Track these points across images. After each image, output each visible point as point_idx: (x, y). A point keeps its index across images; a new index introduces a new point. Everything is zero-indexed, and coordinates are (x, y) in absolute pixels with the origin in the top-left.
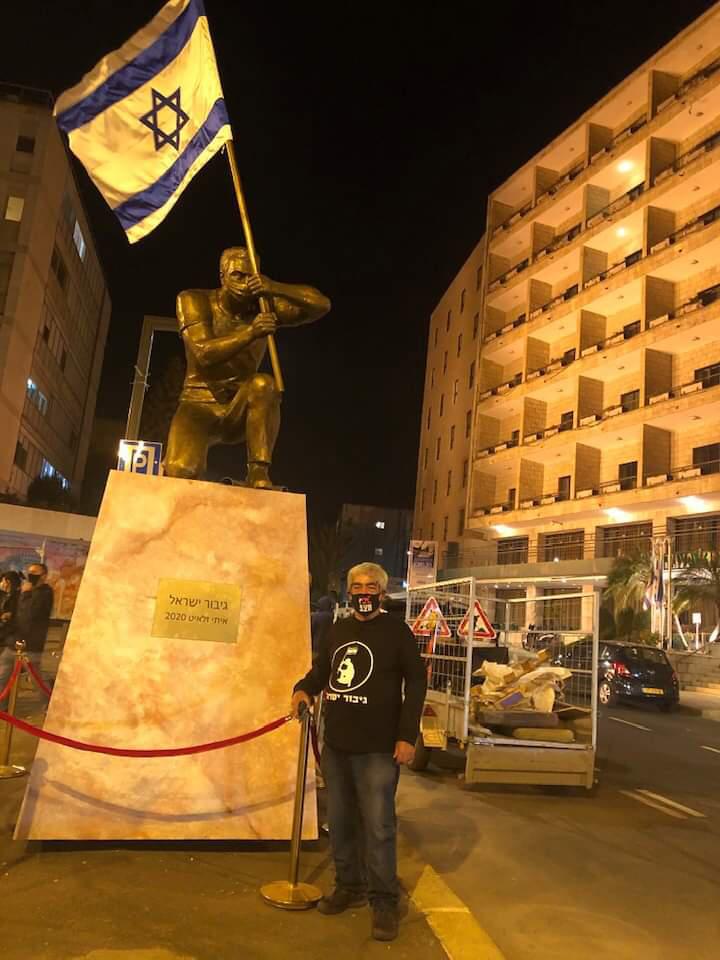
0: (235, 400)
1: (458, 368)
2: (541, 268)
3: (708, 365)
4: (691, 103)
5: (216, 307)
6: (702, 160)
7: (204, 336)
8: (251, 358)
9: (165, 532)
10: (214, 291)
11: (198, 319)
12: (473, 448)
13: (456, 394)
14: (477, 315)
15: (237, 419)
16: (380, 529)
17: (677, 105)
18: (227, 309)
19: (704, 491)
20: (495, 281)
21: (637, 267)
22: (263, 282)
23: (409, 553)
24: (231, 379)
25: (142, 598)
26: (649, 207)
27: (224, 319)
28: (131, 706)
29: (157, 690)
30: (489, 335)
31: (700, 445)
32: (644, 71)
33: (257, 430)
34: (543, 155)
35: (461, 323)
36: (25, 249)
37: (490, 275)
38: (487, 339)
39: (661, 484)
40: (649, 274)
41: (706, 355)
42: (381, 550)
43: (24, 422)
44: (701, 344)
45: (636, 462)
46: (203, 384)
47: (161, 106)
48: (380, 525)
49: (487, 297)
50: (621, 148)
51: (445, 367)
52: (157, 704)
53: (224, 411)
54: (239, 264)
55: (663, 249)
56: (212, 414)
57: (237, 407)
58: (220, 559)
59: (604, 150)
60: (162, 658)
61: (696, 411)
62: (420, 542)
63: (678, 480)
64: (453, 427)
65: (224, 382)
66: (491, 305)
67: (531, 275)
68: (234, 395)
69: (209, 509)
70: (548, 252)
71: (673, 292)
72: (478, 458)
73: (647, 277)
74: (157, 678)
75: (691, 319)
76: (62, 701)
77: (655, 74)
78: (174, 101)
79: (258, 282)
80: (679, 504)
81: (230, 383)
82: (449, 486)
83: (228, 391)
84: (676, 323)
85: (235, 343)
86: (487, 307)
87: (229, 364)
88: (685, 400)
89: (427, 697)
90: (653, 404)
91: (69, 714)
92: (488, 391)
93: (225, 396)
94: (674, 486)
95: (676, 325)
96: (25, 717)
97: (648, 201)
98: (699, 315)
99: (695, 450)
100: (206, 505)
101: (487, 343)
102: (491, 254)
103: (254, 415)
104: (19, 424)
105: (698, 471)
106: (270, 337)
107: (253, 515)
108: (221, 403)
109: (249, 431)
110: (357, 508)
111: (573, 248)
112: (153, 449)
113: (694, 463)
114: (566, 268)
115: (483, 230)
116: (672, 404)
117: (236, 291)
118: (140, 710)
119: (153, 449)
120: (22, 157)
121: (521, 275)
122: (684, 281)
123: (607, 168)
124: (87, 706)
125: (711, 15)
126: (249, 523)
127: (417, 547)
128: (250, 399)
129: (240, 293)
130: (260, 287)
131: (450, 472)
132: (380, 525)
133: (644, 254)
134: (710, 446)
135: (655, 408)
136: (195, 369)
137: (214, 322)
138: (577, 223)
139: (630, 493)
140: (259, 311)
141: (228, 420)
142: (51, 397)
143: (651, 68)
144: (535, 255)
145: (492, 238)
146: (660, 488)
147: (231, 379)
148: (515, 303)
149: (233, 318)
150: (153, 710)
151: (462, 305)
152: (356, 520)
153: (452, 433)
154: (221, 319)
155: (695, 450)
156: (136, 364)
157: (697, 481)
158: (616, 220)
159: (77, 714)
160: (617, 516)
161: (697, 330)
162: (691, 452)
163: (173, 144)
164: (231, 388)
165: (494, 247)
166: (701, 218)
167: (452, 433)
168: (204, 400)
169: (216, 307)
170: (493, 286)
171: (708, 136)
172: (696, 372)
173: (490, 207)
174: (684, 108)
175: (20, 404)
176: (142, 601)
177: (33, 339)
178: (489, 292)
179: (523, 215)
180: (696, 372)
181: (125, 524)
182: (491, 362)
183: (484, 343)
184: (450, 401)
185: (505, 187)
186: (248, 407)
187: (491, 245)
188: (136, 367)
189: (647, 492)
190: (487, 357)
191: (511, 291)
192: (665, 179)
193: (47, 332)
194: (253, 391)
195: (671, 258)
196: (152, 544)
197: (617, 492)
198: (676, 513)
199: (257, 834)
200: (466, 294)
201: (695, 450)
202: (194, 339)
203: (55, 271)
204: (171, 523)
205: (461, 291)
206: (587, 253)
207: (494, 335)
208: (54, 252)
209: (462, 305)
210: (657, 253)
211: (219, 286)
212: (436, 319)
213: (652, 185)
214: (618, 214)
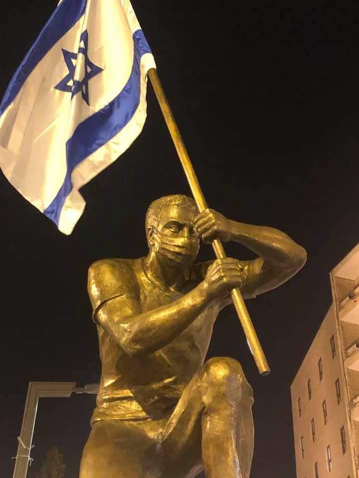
0: (179, 409)
1: (328, 435)
5: (143, 278)
7: (129, 312)
8: (193, 347)
10: (139, 261)
11: (121, 291)
13: (330, 461)
14: (338, 381)
15: (184, 440)
18: (157, 278)
20: (351, 346)
22: (216, 218)
24: (167, 381)
27: (156, 290)
33: (221, 450)
35: (323, 390)
37: (345, 342)
46: (128, 393)
49: (347, 361)
51: (314, 434)
53: (161, 430)
54: (165, 225)
56: (145, 438)
57: (183, 420)
65: (155, 386)
68: (176, 404)
79: (210, 219)
81: (166, 387)
83: (163, 399)
86: (348, 370)
87: (160, 353)
93: (160, 407)
96: (96, 305)
103: (213, 426)
106: (235, 291)
108: (154, 419)
109: (209, 452)
115: (330, 301)
117: (171, 249)
128: (206, 399)
129: (177, 250)
130: (213, 225)
136: (114, 370)
137: (142, 297)
140: (215, 258)
141: (168, 443)
145: (340, 308)
147: (167, 381)
149: (167, 290)
151: (321, 373)
154: (151, 291)
156: (19, 435)
164: (169, 395)
165: (342, 316)
168: (128, 416)
169: (143, 278)
170: (350, 350)
173: (333, 284)
178: (348, 357)
186: (204, 412)
187: (340, 314)
188: (19, 438)
194: (212, 384)
200: (323, 362)
202: (116, 319)
205: (318, 361)
209: (321, 373)
211: (145, 251)
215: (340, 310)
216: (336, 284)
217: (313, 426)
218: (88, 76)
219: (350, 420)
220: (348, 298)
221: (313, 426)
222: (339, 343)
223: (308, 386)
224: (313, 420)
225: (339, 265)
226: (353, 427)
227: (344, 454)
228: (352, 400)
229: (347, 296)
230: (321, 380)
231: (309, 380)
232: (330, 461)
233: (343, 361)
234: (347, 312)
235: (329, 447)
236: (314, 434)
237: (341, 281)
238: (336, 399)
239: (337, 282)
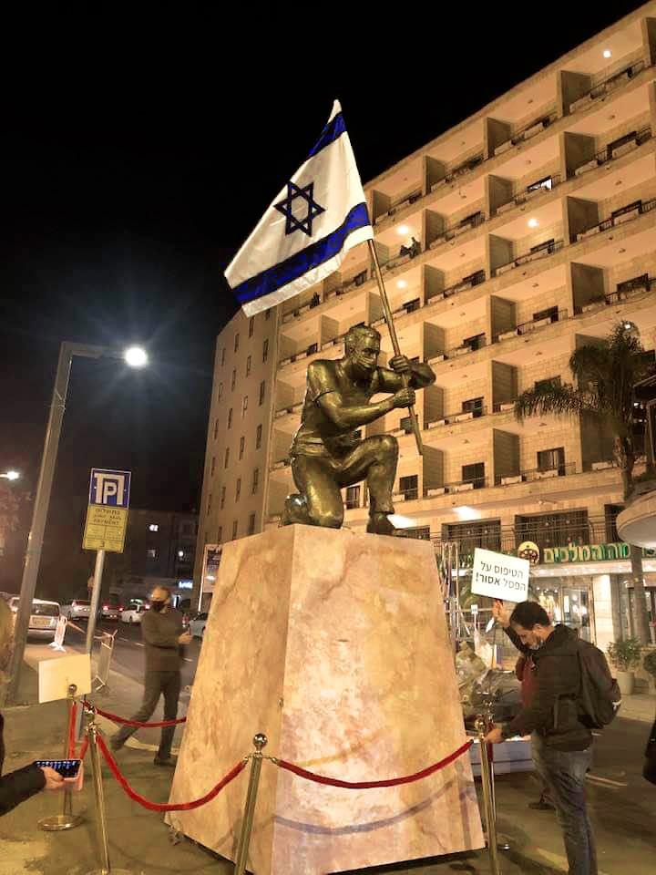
2: (330, 307)
3: (473, 398)
4: (459, 187)
6: (468, 234)
9: (342, 580)
12: (269, 459)
13: (245, 409)
17: (447, 188)
19: (476, 502)
21: (417, 313)
25: (334, 641)
26: (426, 266)
28: (340, 744)
29: (357, 726)
31: (468, 464)
32: (419, 155)
38: (282, 364)
39: (440, 495)
40: (427, 321)
41: (472, 390)
44: (468, 380)
45: (416, 476)
46: (319, 440)
47: (295, 196)
48: (154, 528)
50: (401, 214)
52: (357, 737)
55: (439, 301)
58: (383, 602)
59: (387, 214)
60: (357, 696)
61: (466, 436)
62: (215, 546)
63: (454, 493)
67: (323, 311)
69: (369, 557)
70: (338, 294)
71: (444, 337)
72: (274, 469)
73: (425, 323)
74: (355, 714)
75: (462, 360)
76: (289, 744)
77: (428, 158)
78: (308, 193)
80: (452, 513)
82: (238, 492)
84: (449, 363)
85: (378, 410)
88: (458, 427)
90: (432, 428)
91: (295, 755)
92: (284, 409)
94: (450, 497)
95: (449, 364)
97: (425, 261)
98: (468, 358)
99: (464, 468)
100: (367, 553)
101: (281, 368)
105: (471, 486)
107: (401, 562)
111: (361, 292)
112: (123, 477)
113: (463, 479)
114: (352, 309)
116: (448, 429)
118: (347, 746)
119: (123, 477)
121: (313, 310)
122: (453, 328)
123: (390, 229)
124: (309, 747)
125: (477, 119)
126: (400, 569)
127: (212, 549)
132: (154, 528)
133: (422, 304)
134: (476, 465)
135: (433, 432)
138: (364, 270)
139: (413, 504)
143: (425, 154)
144: (326, 295)
146: (438, 500)
148: (309, 334)
150: (357, 743)
153: (242, 445)
155: (464, 468)
157: (470, 494)
158: (398, 274)
159: (302, 755)
160: (466, 514)
161: (466, 370)
162: (461, 469)
163: (304, 230)
166: (466, 280)
167: (242, 445)
171: (470, 214)
172: (464, 403)
174: (452, 191)
176: (335, 645)
178: (284, 323)
180: (464, 403)
181: (313, 574)
183: (279, 367)
184: (238, 415)
189: (428, 502)
191: (303, 324)
192: (440, 245)
195: (445, 309)
196: (334, 591)
197: (401, 501)
198: (449, 520)
199: (445, 849)
201: (463, 467)
204: (345, 571)
206: (324, 318)
210: (433, 304)
213: (428, 248)
214: (399, 268)
230: (250, 336)
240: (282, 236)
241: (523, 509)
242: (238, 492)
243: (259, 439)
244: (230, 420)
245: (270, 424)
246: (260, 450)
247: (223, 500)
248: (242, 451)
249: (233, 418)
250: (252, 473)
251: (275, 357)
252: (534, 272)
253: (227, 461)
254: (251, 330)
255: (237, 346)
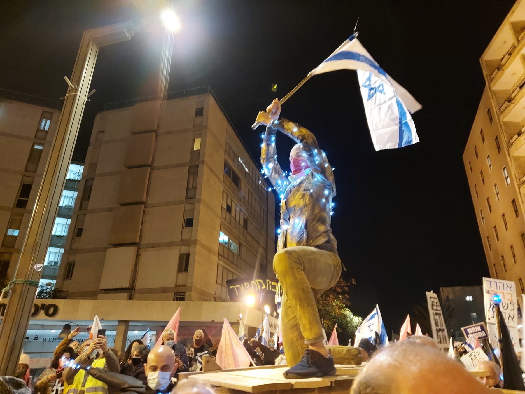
13: (498, 194)
16: (469, 301)
23: (263, 136)
30: (512, 138)
34: (513, 12)
35: (486, 149)
36: (203, 162)
37: (499, 104)
38: (512, 141)
42: (474, 314)
43: (220, 257)
51: (483, 180)
64: (503, 215)
66: (505, 120)
82: (514, 256)
89: (393, 145)
102: (493, 91)
104: (217, 259)
110: (450, 289)
120: (198, 120)
131: (512, 247)
142: (240, 245)
152: (451, 297)
165: (494, 86)
173: (483, 65)
175: (216, 248)
177: (219, 211)
178: (502, 112)
179: (510, 54)
182: (520, 157)
183: (510, 145)
184: (494, 200)
185: (490, 47)
187: (492, 85)
190: (515, 154)
193: (229, 209)
203: (230, 176)
207: (516, 136)
208: (225, 163)
212: (468, 156)
215: (491, 82)
216: (486, 65)
217: (482, 177)
218: (56, 339)
219: (520, 195)
220: (496, 70)
221: (482, 177)
222: (493, 105)
223: (475, 151)
224: (481, 172)
225: (487, 49)
226: (512, 160)
227: (517, 217)
228: (509, 142)
229: (505, 101)
230: (484, 142)
231: (488, 199)
232: (498, 194)
233: (498, 117)
234: (495, 83)
235: (496, 184)
236: (483, 180)
237: (489, 63)
238: (497, 150)
239: (486, 63)
240: (153, 347)
241: (268, 159)
242: (514, 256)
243: (516, 211)
244: (490, 207)
245: (497, 121)
246: (519, 218)
247: (505, 265)
248: (506, 224)
249: (491, 204)
250: (511, 204)
251: (504, 140)
252: (320, 307)
253: (497, 236)
254: (483, 139)
255: (477, 155)
